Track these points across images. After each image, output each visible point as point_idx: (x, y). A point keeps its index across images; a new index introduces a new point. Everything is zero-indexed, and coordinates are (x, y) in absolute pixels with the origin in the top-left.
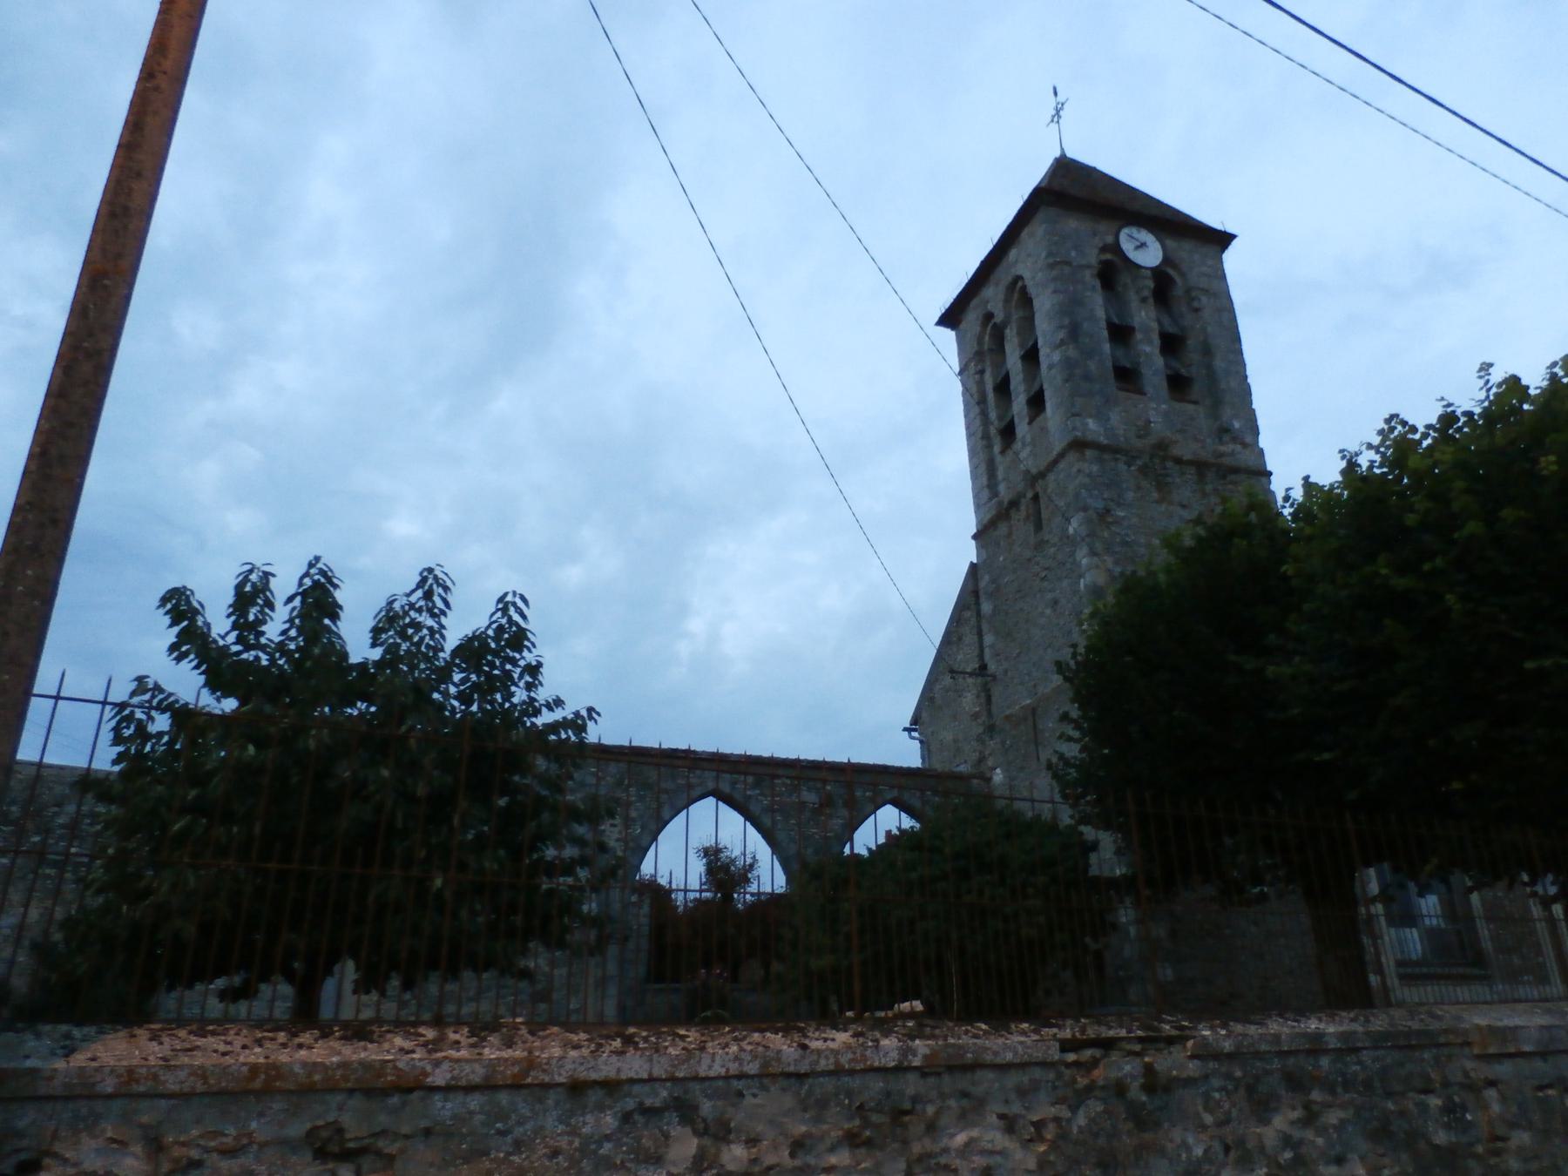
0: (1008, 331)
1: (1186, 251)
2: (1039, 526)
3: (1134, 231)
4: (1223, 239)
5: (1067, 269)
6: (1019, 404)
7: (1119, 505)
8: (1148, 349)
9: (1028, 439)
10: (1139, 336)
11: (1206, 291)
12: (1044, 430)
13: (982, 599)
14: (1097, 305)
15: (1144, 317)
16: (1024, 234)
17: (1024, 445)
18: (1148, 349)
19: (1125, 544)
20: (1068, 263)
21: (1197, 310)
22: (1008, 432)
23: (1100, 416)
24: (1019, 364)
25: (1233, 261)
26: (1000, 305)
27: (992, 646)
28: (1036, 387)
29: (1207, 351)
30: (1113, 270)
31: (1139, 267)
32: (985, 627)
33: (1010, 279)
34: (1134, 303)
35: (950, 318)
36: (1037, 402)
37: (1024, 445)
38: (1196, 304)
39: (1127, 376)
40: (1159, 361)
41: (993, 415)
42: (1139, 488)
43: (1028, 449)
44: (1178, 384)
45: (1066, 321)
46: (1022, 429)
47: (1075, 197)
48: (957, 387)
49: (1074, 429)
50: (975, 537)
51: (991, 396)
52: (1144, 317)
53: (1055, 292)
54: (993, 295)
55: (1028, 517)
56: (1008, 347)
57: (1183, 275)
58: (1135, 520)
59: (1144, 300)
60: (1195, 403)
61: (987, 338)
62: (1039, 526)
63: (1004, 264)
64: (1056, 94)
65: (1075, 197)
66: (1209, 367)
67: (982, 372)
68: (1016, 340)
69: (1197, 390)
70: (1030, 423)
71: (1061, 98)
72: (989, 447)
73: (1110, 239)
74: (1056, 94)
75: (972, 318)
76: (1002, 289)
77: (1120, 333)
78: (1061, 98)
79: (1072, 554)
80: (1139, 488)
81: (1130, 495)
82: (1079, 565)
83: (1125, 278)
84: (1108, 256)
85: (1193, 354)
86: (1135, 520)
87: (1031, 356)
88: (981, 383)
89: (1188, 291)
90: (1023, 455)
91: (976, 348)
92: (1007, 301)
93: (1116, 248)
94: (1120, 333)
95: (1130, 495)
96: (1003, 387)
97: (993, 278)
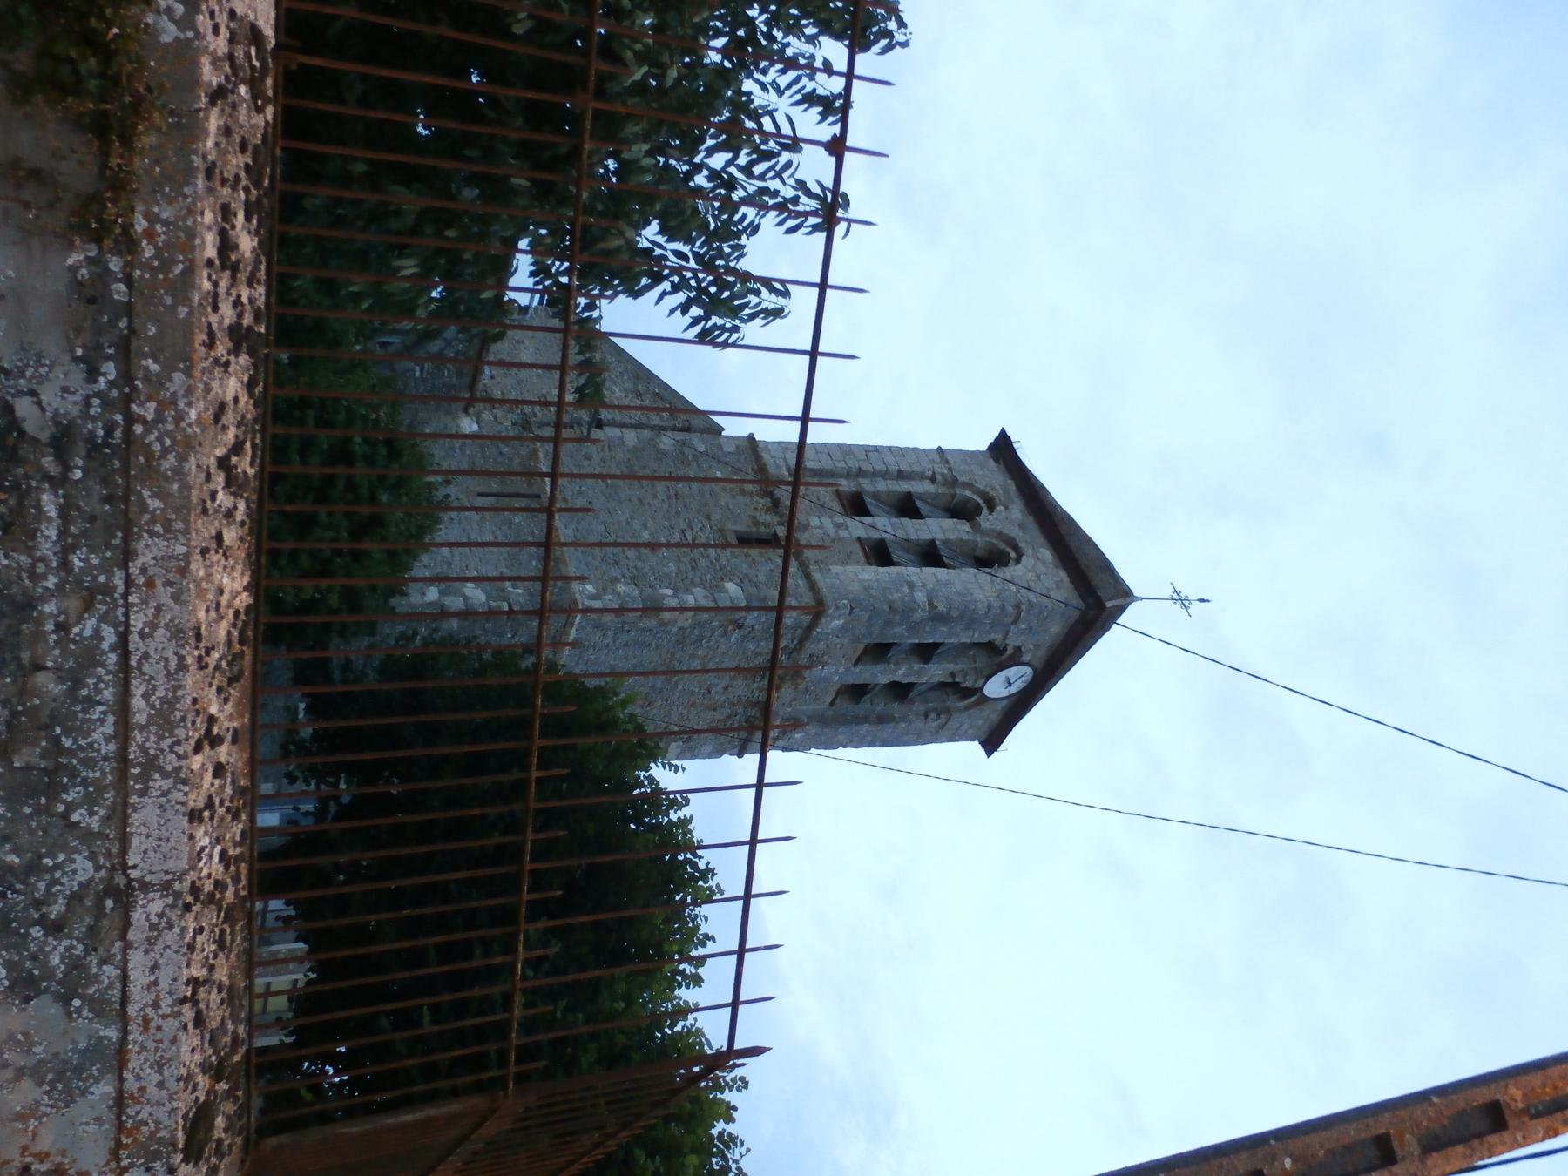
0: (966, 527)
1: (992, 715)
2: (745, 541)
3: (1028, 678)
4: (992, 744)
5: (1009, 620)
6: (885, 526)
7: (744, 637)
8: (901, 672)
9: (843, 534)
10: (916, 666)
11: (943, 726)
12: (847, 559)
13: (680, 436)
14: (965, 601)
15: (937, 671)
16: (1063, 575)
17: (838, 526)
18: (901, 672)
19: (701, 638)
20: (1015, 622)
21: (926, 715)
22: (856, 506)
23: (844, 629)
24: (926, 536)
25: (972, 749)
26: (998, 526)
27: (622, 440)
28: (896, 555)
29: (882, 720)
30: (997, 656)
31: (988, 678)
32: (646, 433)
33: (1022, 545)
34: (951, 667)
35: (1003, 448)
36: (880, 554)
37: (838, 526)
38: (933, 715)
39: (879, 652)
40: (885, 680)
41: (882, 486)
42: (757, 655)
43: (832, 531)
44: (857, 691)
45: (955, 614)
46: (857, 528)
47: (1094, 597)
48: (927, 442)
49: (837, 608)
50: (751, 437)
51: (905, 487)
52: (937, 671)
53: (990, 607)
54: (1009, 518)
55: (756, 523)
56: (949, 523)
57: (967, 708)
58: (723, 648)
59: (953, 675)
60: (832, 704)
61: (968, 493)
62: (745, 541)
63: (1041, 540)
64: (1202, 600)
65: (1094, 597)
66: (866, 719)
67: (933, 480)
68: (953, 536)
69: (846, 706)
70: (859, 539)
71: (1196, 607)
72: (848, 475)
73: (1026, 658)
74: (1202, 600)
75: (995, 480)
76: (1015, 532)
77: (926, 652)
78: (1196, 607)
79: (702, 584)
80: (757, 655)
81: (751, 646)
82: (688, 591)
83: (982, 660)
84: (1010, 651)
85: (899, 634)
86: (723, 648)
87: (930, 555)
88: (921, 476)
89: (948, 711)
90: (826, 520)
91: (961, 479)
92: (1000, 535)
93: (1015, 661)
94: (926, 652)
95: (751, 646)
96: (907, 507)
97: (1031, 522)
